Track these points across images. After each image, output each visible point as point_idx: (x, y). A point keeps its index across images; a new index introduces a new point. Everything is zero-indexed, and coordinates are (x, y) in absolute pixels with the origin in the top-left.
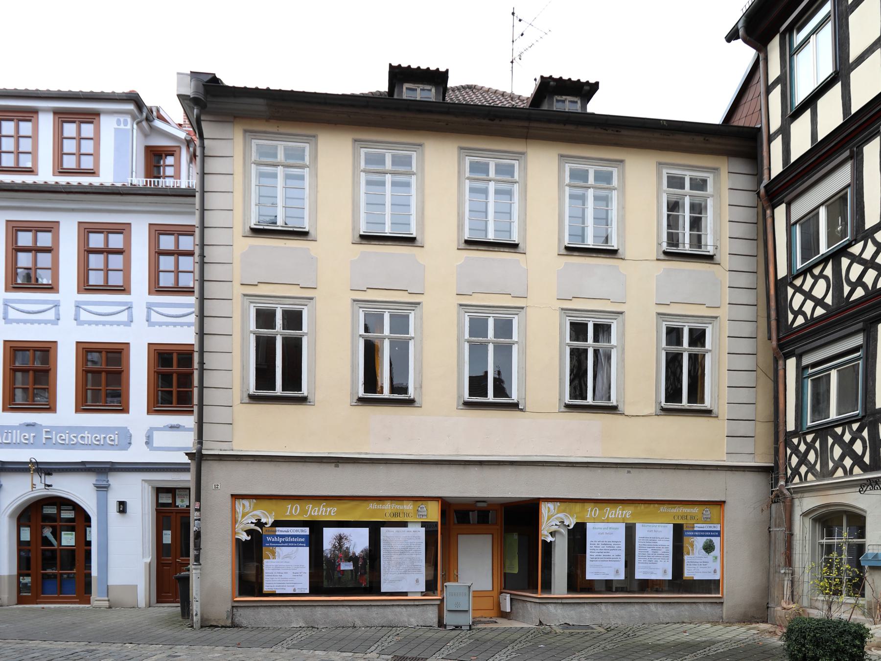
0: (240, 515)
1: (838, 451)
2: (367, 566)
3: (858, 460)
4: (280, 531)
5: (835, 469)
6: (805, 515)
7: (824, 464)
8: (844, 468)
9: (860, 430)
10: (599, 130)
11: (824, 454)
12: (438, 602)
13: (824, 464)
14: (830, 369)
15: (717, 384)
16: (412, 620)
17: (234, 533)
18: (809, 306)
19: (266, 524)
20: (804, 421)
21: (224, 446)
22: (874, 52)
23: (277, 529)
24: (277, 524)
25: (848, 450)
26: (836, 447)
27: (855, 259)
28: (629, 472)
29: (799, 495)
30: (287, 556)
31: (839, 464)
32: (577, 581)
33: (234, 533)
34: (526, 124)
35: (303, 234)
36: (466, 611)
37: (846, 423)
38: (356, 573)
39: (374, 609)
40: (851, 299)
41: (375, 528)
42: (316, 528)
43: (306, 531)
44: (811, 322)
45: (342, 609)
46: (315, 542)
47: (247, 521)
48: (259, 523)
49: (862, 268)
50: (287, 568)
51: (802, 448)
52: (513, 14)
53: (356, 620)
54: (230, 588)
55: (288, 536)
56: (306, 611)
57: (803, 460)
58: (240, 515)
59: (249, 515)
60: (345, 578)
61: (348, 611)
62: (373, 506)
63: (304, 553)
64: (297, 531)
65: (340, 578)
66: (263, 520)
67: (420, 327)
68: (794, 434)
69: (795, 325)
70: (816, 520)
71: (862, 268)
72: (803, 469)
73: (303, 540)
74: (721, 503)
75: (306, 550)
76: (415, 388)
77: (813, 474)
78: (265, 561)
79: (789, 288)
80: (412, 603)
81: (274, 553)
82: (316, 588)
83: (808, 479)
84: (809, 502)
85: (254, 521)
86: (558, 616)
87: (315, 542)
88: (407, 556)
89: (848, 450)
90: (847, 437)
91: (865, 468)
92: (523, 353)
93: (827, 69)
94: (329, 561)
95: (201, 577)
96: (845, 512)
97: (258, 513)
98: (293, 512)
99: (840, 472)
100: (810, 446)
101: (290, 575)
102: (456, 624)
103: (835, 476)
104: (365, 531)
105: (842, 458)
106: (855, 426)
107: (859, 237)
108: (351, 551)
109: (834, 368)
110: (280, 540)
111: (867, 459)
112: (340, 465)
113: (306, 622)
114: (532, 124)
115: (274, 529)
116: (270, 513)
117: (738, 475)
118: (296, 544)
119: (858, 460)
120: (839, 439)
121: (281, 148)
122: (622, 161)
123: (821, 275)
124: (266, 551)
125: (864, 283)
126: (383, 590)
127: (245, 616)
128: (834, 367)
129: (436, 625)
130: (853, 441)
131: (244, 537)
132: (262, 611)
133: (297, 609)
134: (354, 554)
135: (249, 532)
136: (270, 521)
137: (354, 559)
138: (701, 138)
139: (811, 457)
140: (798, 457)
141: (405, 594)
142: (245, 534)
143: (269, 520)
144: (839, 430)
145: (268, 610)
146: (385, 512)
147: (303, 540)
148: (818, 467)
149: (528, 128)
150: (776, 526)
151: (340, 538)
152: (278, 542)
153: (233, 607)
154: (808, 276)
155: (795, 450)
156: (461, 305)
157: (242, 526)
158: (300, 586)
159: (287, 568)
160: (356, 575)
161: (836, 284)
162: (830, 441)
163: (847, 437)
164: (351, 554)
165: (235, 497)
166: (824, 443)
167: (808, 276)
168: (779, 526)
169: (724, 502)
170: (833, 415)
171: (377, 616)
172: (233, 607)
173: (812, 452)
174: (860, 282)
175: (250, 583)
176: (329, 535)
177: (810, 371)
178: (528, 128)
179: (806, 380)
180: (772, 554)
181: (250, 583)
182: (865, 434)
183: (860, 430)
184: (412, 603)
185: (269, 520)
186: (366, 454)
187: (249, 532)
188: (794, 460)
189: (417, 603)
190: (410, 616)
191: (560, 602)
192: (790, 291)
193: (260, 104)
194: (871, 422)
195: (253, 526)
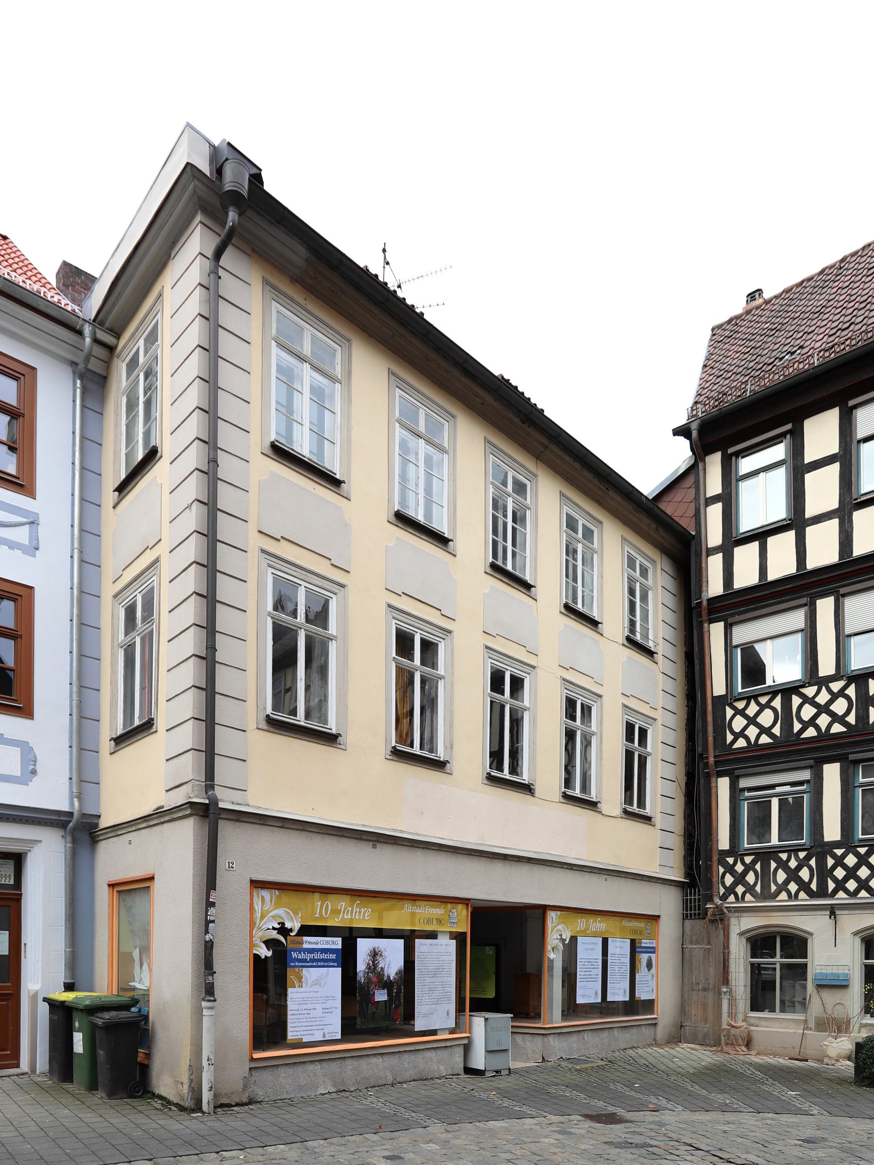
0: (258, 915)
1: (781, 876)
2: (402, 995)
3: (804, 886)
4: (310, 942)
5: (778, 893)
6: (741, 934)
7: (765, 886)
8: (789, 893)
9: (808, 858)
10: (596, 481)
11: (765, 877)
12: (466, 1042)
13: (765, 886)
14: (772, 797)
15: (654, 792)
16: (442, 1068)
17: (252, 945)
18: (752, 732)
19: (291, 930)
20: (741, 843)
21: (236, 796)
22: (831, 519)
23: (305, 938)
24: (306, 930)
25: (793, 875)
26: (780, 871)
27: (806, 700)
28: (606, 880)
29: (737, 914)
30: (316, 983)
31: (783, 887)
32: (571, 1008)
33: (252, 945)
34: (545, 441)
35: (333, 482)
36: (506, 1050)
37: (793, 851)
38: (391, 1005)
39: (406, 1056)
40: (803, 736)
41: (409, 938)
42: (350, 937)
43: (336, 943)
44: (753, 747)
45: (374, 1060)
46: (347, 958)
47: (267, 928)
48: (283, 930)
49: (815, 711)
50: (315, 1003)
51: (739, 868)
52: (384, 251)
53: (388, 1074)
54: (248, 1038)
55: (317, 950)
56: (334, 1066)
57: (740, 879)
58: (258, 915)
59: (275, 914)
60: (376, 1010)
61: (381, 1060)
62: (408, 908)
63: (336, 974)
64: (327, 942)
65: (374, 1013)
66: (288, 925)
67: (450, 664)
68: (730, 853)
69: (735, 746)
70: (748, 940)
71: (815, 711)
72: (740, 889)
73: (334, 956)
74: (656, 918)
75: (339, 970)
76: (445, 747)
77: (752, 895)
78: (290, 990)
79: (727, 708)
80: (443, 1044)
81: (300, 979)
82: (351, 1028)
83: (746, 899)
84: (749, 922)
85: (277, 926)
86: (559, 1048)
87: (347, 958)
88: (439, 979)
89: (793, 875)
90: (793, 864)
91: (811, 894)
92: (534, 723)
93: (779, 512)
94: (362, 987)
95: (215, 1019)
96: (779, 933)
97: (280, 912)
98: (324, 912)
99: (783, 896)
100: (748, 868)
101: (318, 1013)
102: (496, 1068)
103: (778, 899)
104: (401, 942)
105: (787, 882)
106: (802, 855)
107: (813, 681)
108: (386, 974)
109: (776, 796)
110: (309, 956)
111: (814, 886)
112: (378, 845)
113: (335, 1086)
114: (552, 446)
115: (299, 938)
116: (296, 913)
117: (658, 888)
118: (325, 963)
119: (804, 886)
120: (783, 865)
121: (309, 337)
122: (601, 523)
123: (768, 705)
124: (291, 976)
125: (817, 725)
126: (417, 1028)
127: (271, 1084)
128: (776, 795)
129: (462, 1072)
130: (799, 868)
131: (264, 952)
132: (283, 1072)
133: (324, 1065)
134: (389, 977)
135: (269, 943)
136: (296, 926)
137: (387, 985)
138: (654, 526)
139: (750, 878)
140: (733, 876)
141: (434, 1032)
142: (263, 946)
143: (294, 925)
144: (784, 856)
145: (290, 1071)
146: (361, 916)
147: (334, 956)
148: (758, 888)
149: (546, 447)
150: (691, 943)
151: (375, 954)
152: (305, 961)
153: (250, 1069)
154: (753, 702)
155: (730, 869)
156: (487, 647)
157: (260, 934)
158: (327, 1029)
159: (315, 1003)
160: (390, 1008)
161: (786, 716)
162: (773, 865)
163: (793, 864)
164: (386, 978)
165: (256, 884)
166: (765, 867)
167: (753, 702)
168: (697, 942)
169: (659, 916)
170: (775, 840)
171: (408, 1065)
172: (250, 1069)
173: (751, 873)
174: (812, 722)
175: (270, 1027)
176: (364, 946)
177: (747, 794)
178: (546, 447)
179: (742, 802)
180: (686, 972)
181: (270, 1027)
182: (813, 862)
183: (808, 858)
184: (443, 1044)
185: (294, 925)
186: (402, 831)
187: (269, 943)
188: (729, 880)
189: (448, 1044)
190: (439, 1062)
191: (559, 1033)
192: (729, 712)
193: (298, 254)
194: (818, 853)
195: (274, 935)
